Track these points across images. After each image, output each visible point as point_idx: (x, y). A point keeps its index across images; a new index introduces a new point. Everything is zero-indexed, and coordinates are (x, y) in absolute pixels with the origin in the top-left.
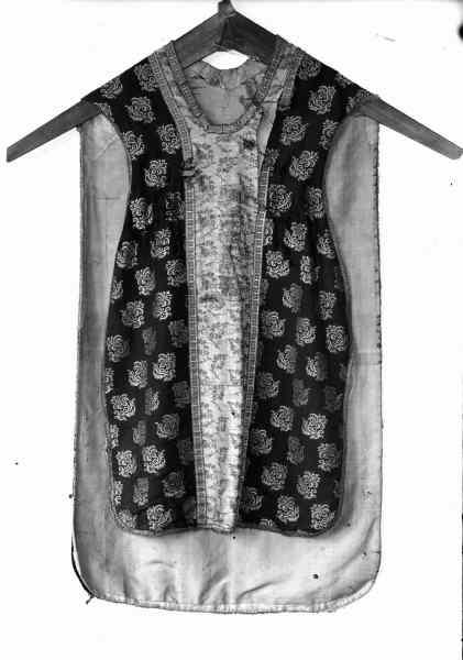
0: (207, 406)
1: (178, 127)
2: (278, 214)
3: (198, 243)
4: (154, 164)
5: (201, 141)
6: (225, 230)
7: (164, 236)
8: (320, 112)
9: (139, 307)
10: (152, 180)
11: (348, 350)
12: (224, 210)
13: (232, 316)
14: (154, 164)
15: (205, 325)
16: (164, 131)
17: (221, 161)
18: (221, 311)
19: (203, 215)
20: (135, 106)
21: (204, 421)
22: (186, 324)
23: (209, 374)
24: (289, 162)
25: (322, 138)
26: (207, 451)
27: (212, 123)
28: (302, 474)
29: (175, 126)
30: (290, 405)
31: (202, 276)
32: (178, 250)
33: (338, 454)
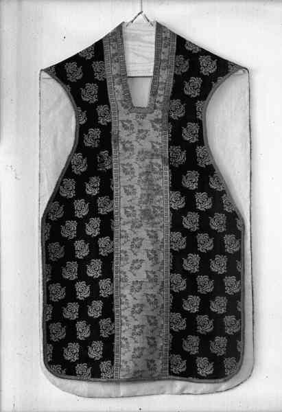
0: (125, 296)
1: (112, 107)
2: (177, 166)
3: (122, 184)
4: (91, 131)
5: (125, 118)
6: (143, 178)
7: (95, 181)
8: (195, 74)
9: (73, 225)
10: (89, 143)
11: (240, 249)
12: (141, 164)
13: (148, 255)
14: (91, 131)
15: (127, 328)
16: (101, 109)
17: (139, 131)
18: (139, 230)
19: (125, 167)
20: (86, 77)
21: (123, 306)
22: (113, 320)
23: (129, 297)
24: (181, 131)
25: (225, 206)
26: (123, 328)
27: (133, 107)
28: (206, 337)
29: (109, 107)
30: (196, 334)
31: (125, 208)
32: (107, 190)
33: (238, 322)
